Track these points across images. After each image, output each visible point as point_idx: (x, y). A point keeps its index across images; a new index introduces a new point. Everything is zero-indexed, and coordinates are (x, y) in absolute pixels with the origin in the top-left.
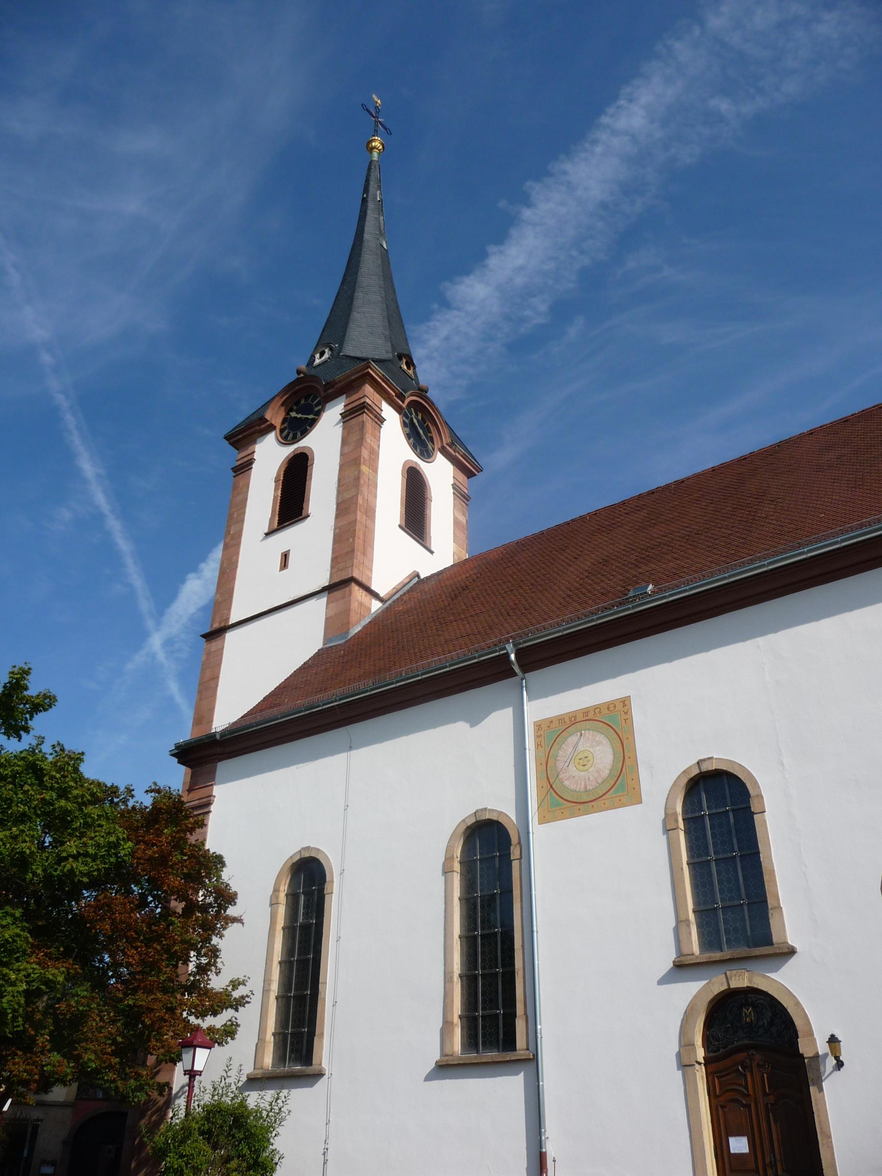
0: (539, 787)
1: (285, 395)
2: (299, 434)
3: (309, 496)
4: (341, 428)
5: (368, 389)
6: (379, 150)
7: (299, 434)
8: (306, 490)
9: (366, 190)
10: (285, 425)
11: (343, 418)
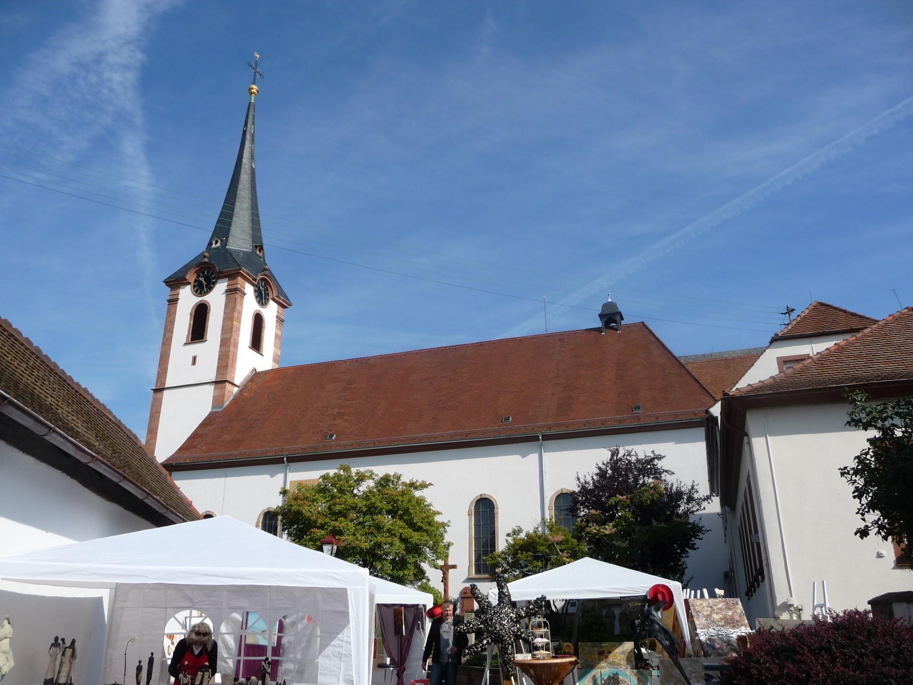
5: (240, 279)
9: (246, 125)
10: (196, 284)
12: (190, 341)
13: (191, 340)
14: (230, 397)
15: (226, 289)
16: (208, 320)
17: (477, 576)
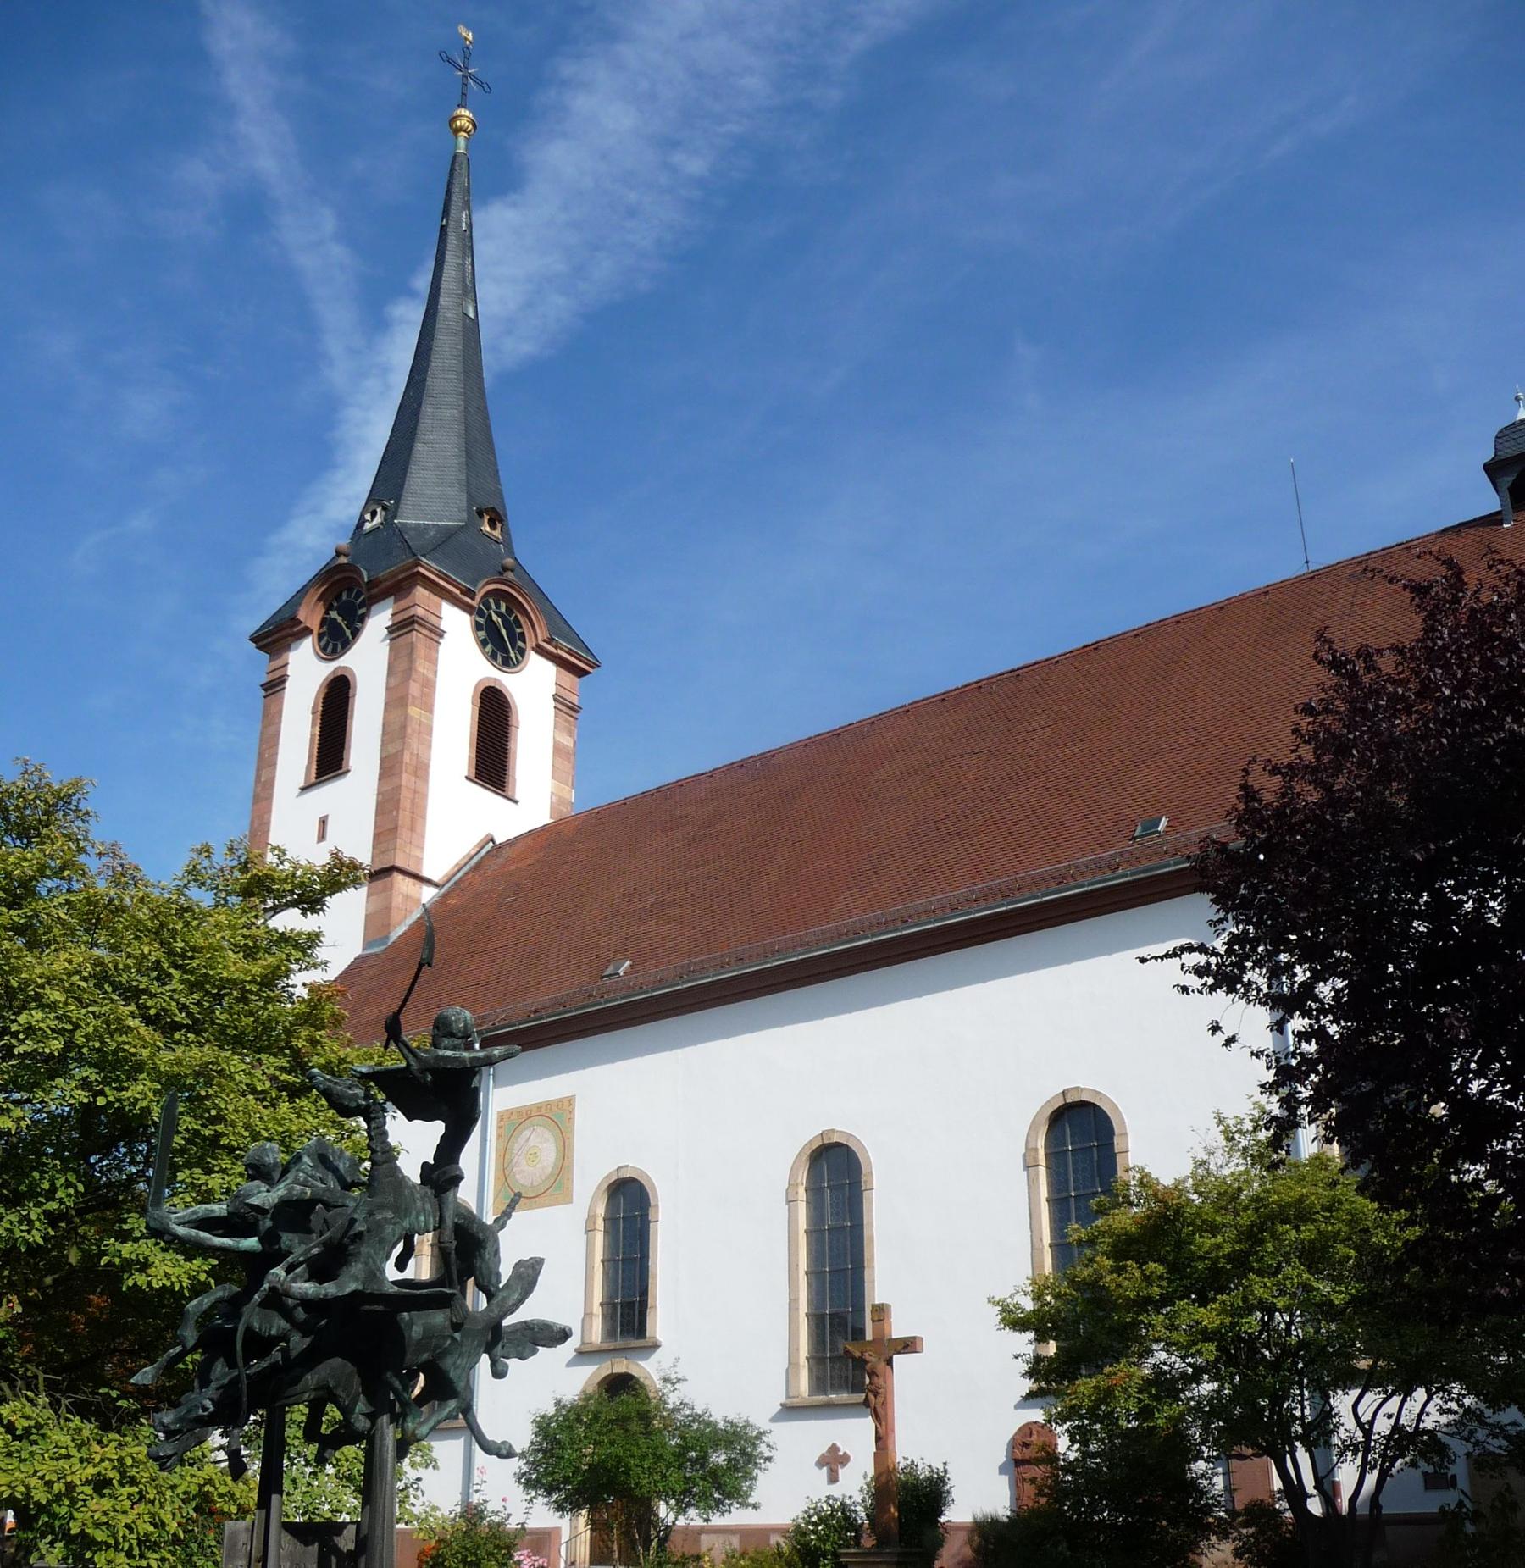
0: (497, 1179)
1: (320, 587)
2: (340, 647)
3: (350, 741)
4: (388, 648)
5: (420, 592)
6: (468, 133)
7: (340, 647)
8: (347, 734)
9: (446, 213)
10: (325, 629)
11: (390, 633)
12: (313, 780)
13: (316, 778)
14: (411, 912)
15: (390, 623)
16: (352, 716)
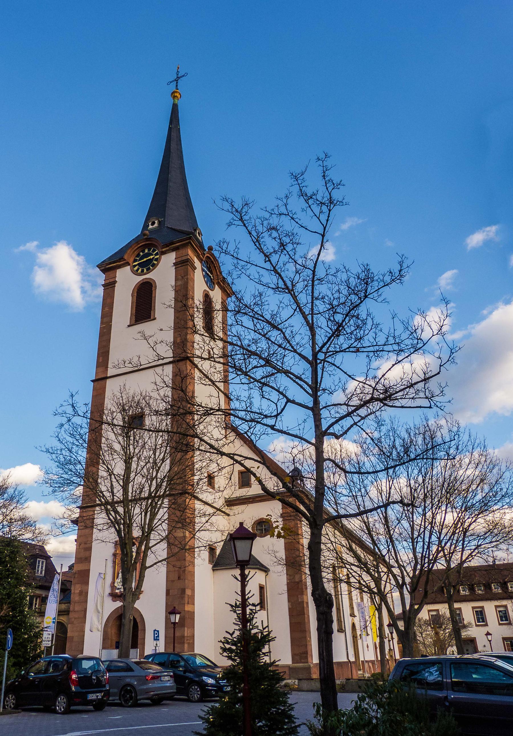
12: (133, 322)
15: (174, 262)
17: (119, 659)
